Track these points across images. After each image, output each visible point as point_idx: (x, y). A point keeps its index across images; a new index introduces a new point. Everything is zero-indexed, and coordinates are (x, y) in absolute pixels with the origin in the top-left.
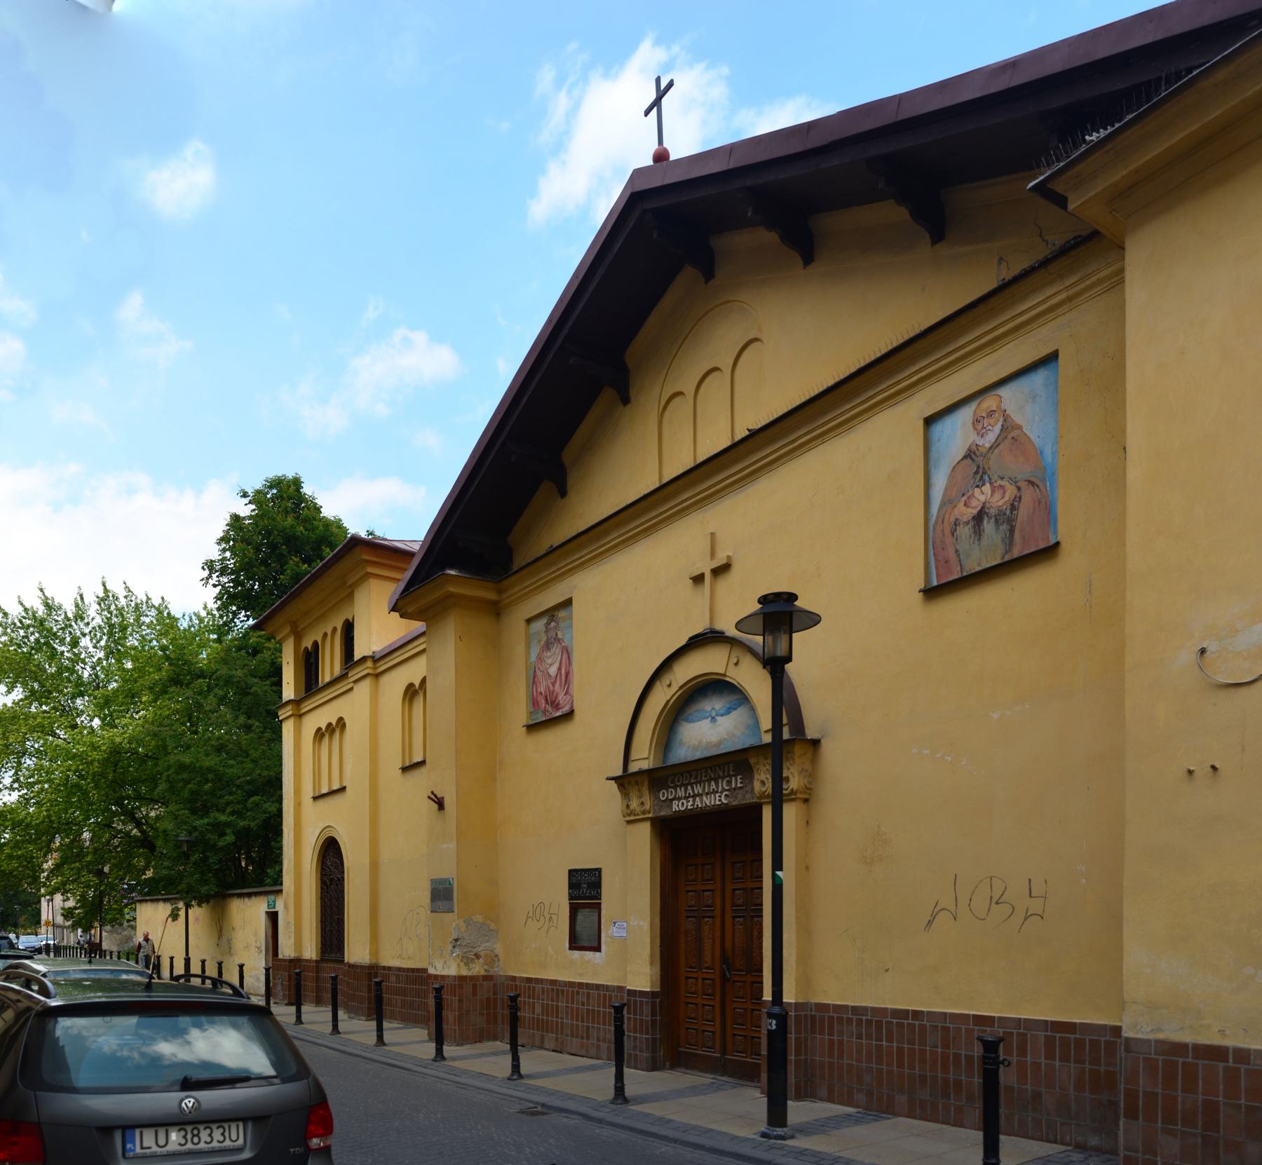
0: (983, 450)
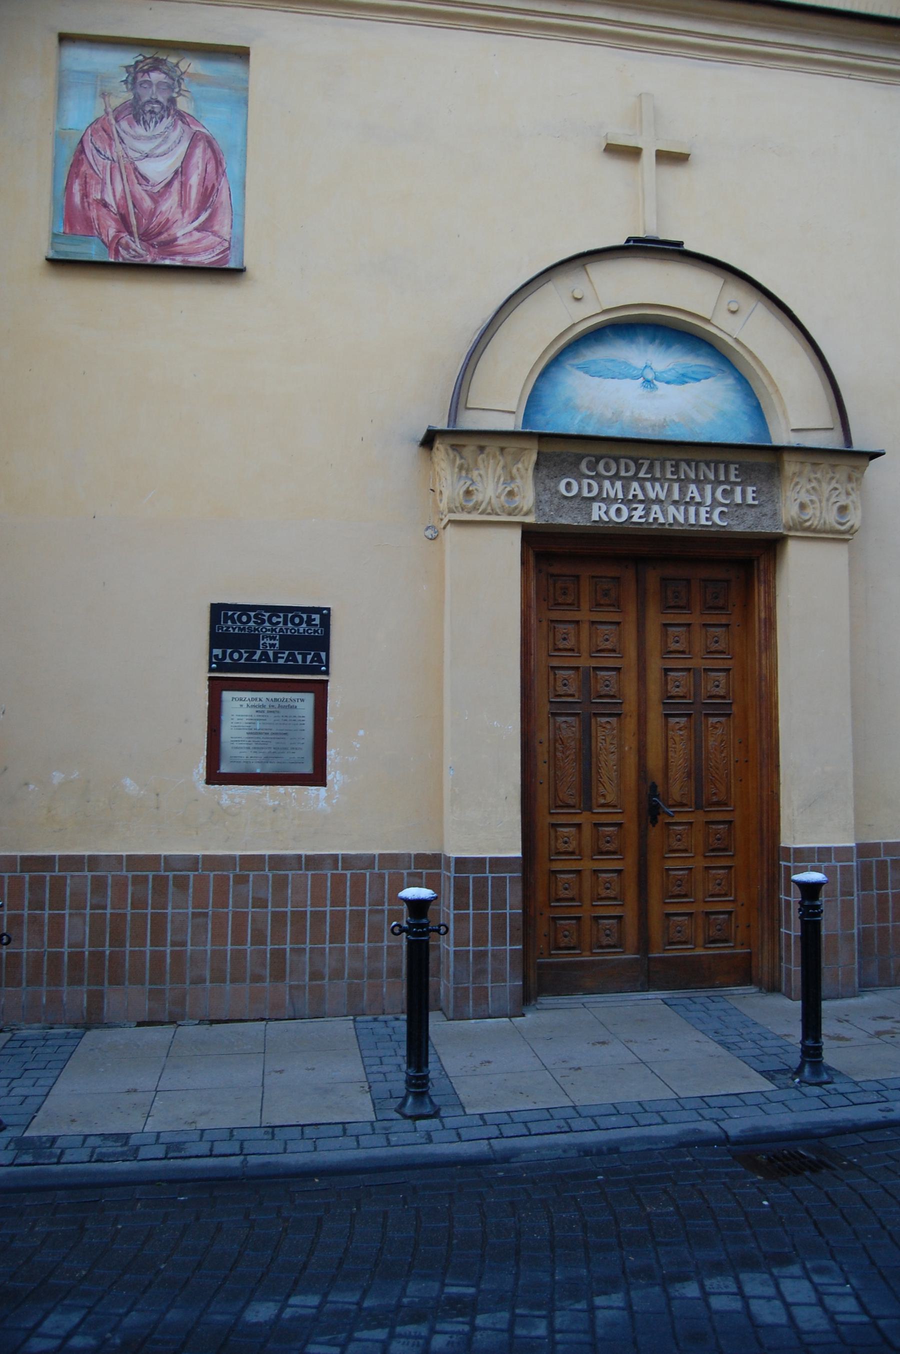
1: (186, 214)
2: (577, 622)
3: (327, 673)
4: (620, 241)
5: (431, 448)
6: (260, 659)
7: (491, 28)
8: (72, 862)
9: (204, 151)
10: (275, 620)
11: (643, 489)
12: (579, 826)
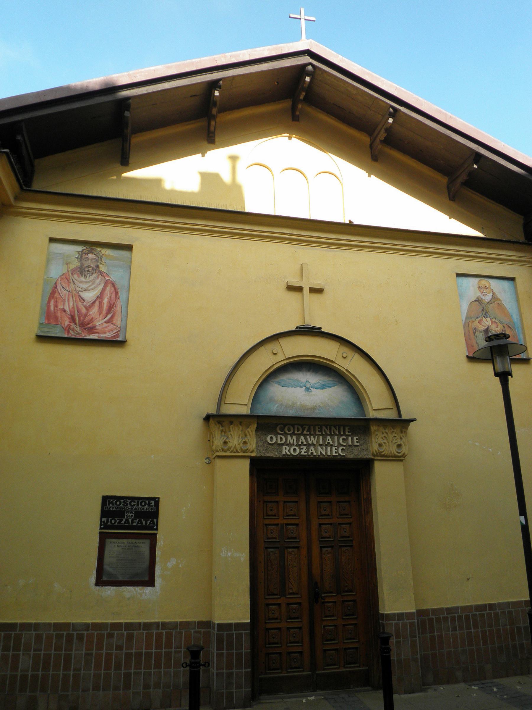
0: (486, 303)
1: (101, 316)
2: (277, 502)
3: (157, 529)
4: (293, 328)
5: (209, 421)
6: (125, 523)
7: (237, 237)
8: (25, 626)
9: (111, 288)
10: (133, 503)
11: (306, 439)
12: (279, 605)
